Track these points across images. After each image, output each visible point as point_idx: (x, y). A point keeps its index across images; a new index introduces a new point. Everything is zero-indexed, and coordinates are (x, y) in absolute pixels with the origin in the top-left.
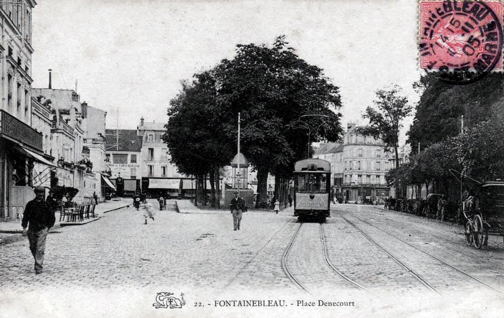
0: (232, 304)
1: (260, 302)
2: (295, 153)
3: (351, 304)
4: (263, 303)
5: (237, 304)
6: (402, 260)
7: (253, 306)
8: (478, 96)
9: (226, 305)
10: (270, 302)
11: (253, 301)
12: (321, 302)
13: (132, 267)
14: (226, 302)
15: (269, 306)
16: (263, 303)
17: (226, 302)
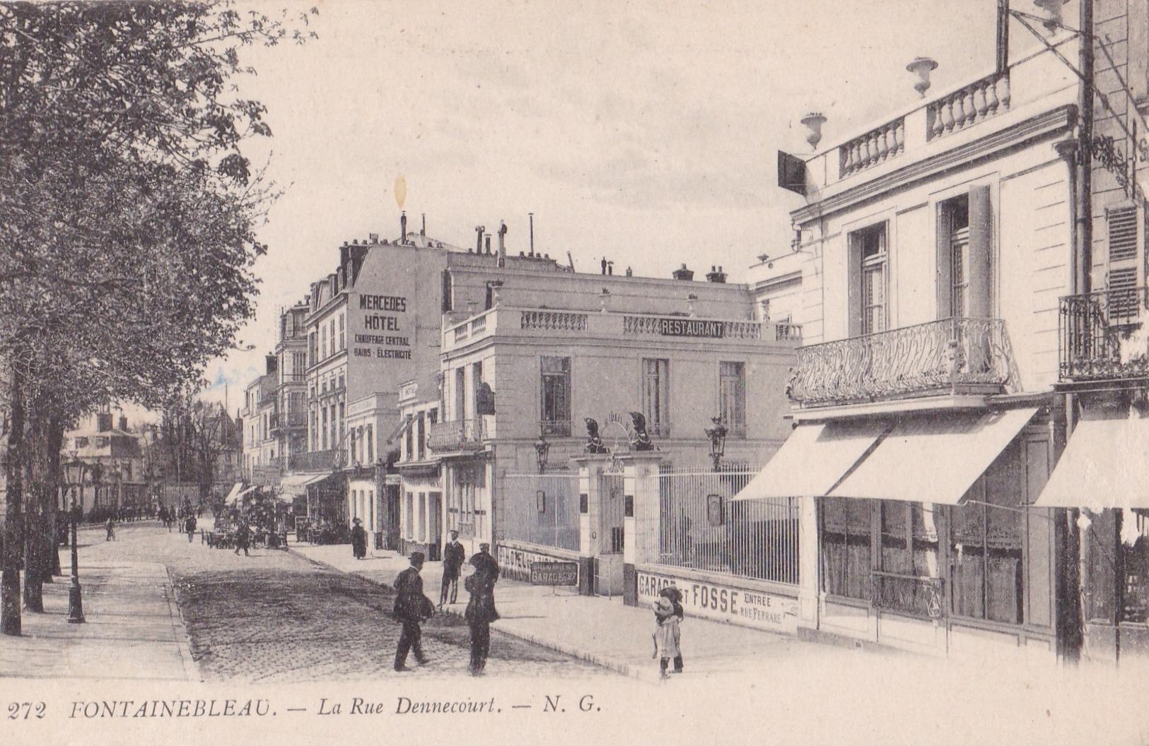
0: (119, 710)
1: (201, 704)
3: (486, 708)
9: (100, 713)
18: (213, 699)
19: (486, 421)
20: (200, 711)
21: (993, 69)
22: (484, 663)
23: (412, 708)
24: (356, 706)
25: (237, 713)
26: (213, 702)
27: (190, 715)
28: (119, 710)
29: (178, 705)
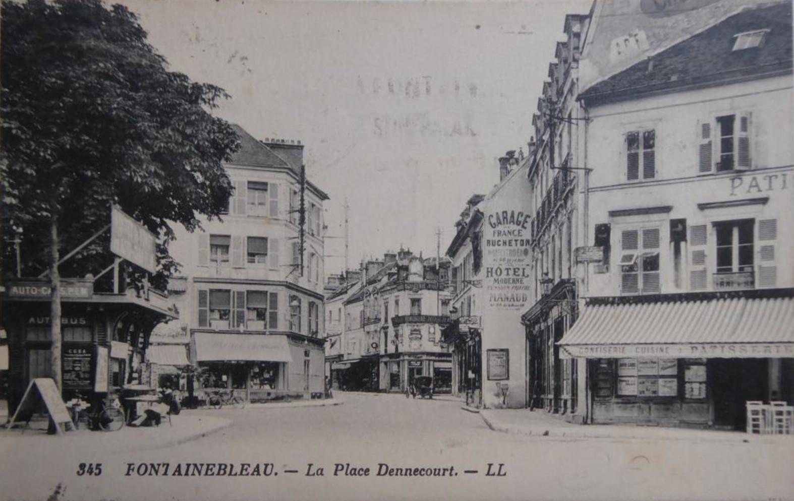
0: (162, 470)
1: (223, 467)
2: (101, 248)
3: (447, 473)
4: (228, 470)
5: (171, 470)
6: (553, 227)
7: (206, 474)
8: (186, 84)
9: (148, 472)
10: (246, 467)
11: (208, 465)
12: (384, 468)
13: (663, 384)
14: (149, 467)
15: (241, 474)
16: (228, 470)
17: (149, 467)
18: (310, 463)
19: (673, 381)
20: (222, 472)
21: (196, 334)
22: (221, 126)
23: (390, 472)
24: (338, 468)
25: (251, 473)
26: (501, 465)
27: (215, 474)
28: (162, 470)
29: (205, 467)
